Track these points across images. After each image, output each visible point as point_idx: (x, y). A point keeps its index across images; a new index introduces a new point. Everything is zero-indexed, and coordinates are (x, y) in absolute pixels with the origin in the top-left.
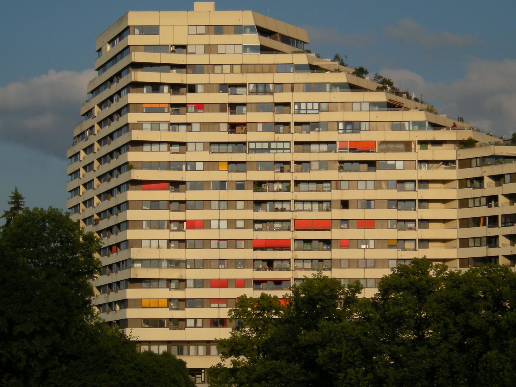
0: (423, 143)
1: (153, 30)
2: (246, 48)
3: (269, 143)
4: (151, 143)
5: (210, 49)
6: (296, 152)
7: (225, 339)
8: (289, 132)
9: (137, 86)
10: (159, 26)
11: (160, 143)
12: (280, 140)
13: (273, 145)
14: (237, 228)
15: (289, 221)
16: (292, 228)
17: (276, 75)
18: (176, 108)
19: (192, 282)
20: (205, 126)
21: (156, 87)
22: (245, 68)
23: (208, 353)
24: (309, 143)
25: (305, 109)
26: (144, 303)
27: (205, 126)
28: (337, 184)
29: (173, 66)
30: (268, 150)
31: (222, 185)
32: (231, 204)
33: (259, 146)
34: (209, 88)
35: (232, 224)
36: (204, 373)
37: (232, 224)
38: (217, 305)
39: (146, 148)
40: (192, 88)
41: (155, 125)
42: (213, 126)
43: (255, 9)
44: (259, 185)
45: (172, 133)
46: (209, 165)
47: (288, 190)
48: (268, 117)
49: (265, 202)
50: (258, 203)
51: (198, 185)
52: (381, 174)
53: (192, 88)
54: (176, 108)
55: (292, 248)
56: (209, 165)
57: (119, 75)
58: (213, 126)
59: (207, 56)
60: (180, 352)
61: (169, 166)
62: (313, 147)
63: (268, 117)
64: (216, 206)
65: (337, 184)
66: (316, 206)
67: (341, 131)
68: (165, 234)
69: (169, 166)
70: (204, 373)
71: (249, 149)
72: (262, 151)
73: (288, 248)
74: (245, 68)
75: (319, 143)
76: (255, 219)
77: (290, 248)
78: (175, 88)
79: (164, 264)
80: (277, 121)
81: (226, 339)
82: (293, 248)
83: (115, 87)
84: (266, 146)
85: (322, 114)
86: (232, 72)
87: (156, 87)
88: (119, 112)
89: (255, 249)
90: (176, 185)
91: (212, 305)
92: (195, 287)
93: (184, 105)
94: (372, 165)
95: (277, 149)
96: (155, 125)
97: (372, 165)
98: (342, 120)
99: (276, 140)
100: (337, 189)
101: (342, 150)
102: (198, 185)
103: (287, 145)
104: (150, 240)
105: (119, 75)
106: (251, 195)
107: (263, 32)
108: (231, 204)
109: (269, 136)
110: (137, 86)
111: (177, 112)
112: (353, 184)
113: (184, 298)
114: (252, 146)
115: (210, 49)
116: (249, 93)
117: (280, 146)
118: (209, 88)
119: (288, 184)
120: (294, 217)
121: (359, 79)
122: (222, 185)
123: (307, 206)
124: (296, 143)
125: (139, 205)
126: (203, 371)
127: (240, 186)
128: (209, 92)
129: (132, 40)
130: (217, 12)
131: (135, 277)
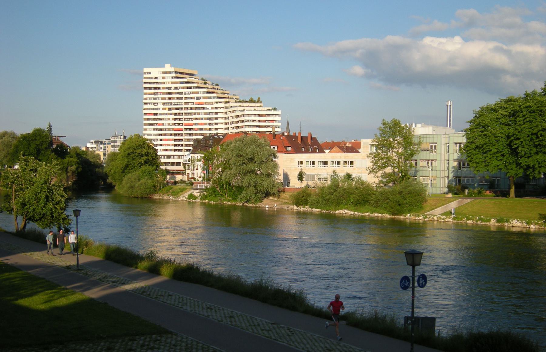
0: (217, 102)
1: (150, 73)
2: (172, 78)
4: (149, 103)
5: (164, 78)
11: (151, 103)
13: (179, 103)
18: (155, 94)
20: (163, 99)
21: (150, 88)
22: (173, 83)
24: (189, 103)
26: (178, 140)
27: (163, 99)
28: (195, 114)
30: (177, 105)
31: (166, 114)
32: (169, 119)
33: (175, 104)
34: (163, 88)
35: (169, 124)
37: (169, 124)
40: (159, 88)
41: (150, 99)
42: (164, 99)
43: (174, 67)
45: (155, 100)
46: (164, 109)
47: (182, 115)
51: (161, 114)
52: (205, 111)
53: (159, 88)
54: (155, 94)
56: (164, 109)
58: (164, 99)
61: (153, 109)
62: (190, 104)
64: (533, 200)
65: (195, 114)
66: (190, 119)
68: (153, 127)
69: (153, 109)
72: (176, 105)
74: (173, 83)
75: (191, 103)
78: (155, 88)
82: (442, 147)
84: (177, 103)
85: (191, 95)
86: (169, 82)
87: (150, 88)
89: (175, 131)
90: (155, 114)
93: (157, 93)
94: (204, 108)
96: (150, 99)
97: (204, 108)
101: (196, 104)
102: (161, 114)
107: (176, 72)
108: (169, 119)
109: (178, 101)
111: (156, 95)
112: (199, 114)
114: (174, 103)
115: (164, 78)
118: (163, 88)
121: (217, 115)
122: (166, 114)
123: (188, 119)
127: (171, 114)
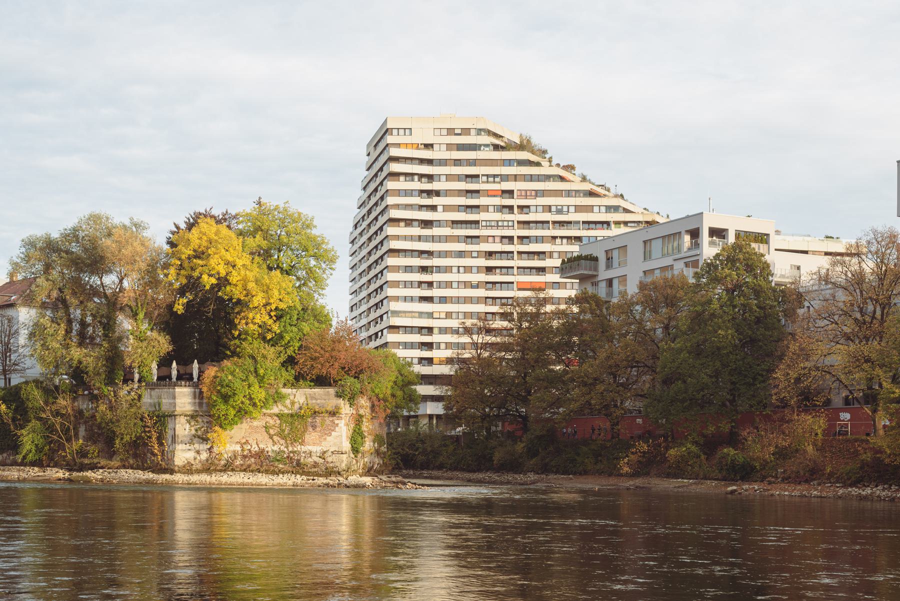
3: (498, 221)
6: (518, 229)
8: (513, 244)
9: (395, 175)
12: (506, 219)
13: (500, 224)
14: (472, 257)
15: (513, 283)
16: (515, 289)
19: (442, 207)
29: (422, 252)
39: (402, 178)
44: (490, 254)
48: (497, 201)
49: (496, 268)
50: (489, 270)
57: (381, 169)
59: (449, 152)
63: (497, 201)
71: (482, 226)
76: (487, 281)
80: (503, 204)
83: (379, 253)
88: (382, 242)
92: (440, 303)
95: (503, 226)
99: (503, 219)
100: (550, 258)
103: (510, 224)
105: (381, 169)
106: (484, 262)
109: (498, 216)
110: (395, 175)
116: (482, 182)
117: (506, 224)
119: (511, 255)
120: (517, 280)
124: (519, 222)
125: (397, 269)
128: (451, 150)
129: (390, 200)
131: (393, 324)
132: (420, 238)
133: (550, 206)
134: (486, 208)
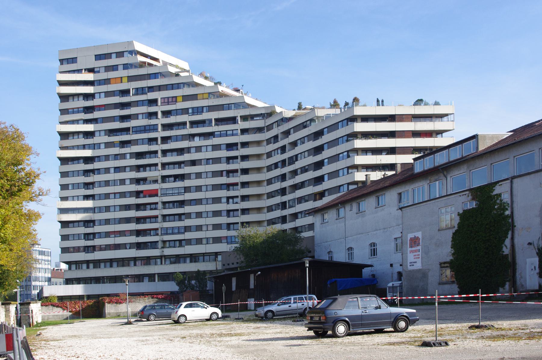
7: (458, 287)
10: (77, 58)
17: (149, 81)
23: (88, 267)
25: (167, 101)
31: (116, 157)
36: (102, 279)
38: (114, 236)
46: (108, 145)
55: (159, 195)
60: (77, 267)
67: (191, 114)
70: (102, 279)
73: (157, 195)
77: (158, 194)
79: (128, 195)
81: (458, 286)
91: (111, 236)
98: (191, 107)
104: (73, 196)
113: (93, 232)
126: (105, 278)
130: (117, 59)
132: (84, 147)
133: (188, 109)
134: (135, 117)
